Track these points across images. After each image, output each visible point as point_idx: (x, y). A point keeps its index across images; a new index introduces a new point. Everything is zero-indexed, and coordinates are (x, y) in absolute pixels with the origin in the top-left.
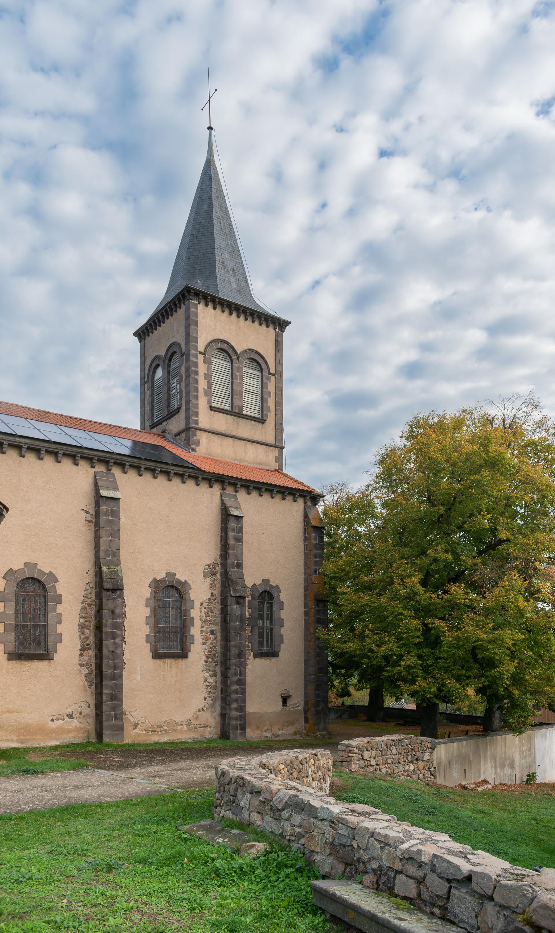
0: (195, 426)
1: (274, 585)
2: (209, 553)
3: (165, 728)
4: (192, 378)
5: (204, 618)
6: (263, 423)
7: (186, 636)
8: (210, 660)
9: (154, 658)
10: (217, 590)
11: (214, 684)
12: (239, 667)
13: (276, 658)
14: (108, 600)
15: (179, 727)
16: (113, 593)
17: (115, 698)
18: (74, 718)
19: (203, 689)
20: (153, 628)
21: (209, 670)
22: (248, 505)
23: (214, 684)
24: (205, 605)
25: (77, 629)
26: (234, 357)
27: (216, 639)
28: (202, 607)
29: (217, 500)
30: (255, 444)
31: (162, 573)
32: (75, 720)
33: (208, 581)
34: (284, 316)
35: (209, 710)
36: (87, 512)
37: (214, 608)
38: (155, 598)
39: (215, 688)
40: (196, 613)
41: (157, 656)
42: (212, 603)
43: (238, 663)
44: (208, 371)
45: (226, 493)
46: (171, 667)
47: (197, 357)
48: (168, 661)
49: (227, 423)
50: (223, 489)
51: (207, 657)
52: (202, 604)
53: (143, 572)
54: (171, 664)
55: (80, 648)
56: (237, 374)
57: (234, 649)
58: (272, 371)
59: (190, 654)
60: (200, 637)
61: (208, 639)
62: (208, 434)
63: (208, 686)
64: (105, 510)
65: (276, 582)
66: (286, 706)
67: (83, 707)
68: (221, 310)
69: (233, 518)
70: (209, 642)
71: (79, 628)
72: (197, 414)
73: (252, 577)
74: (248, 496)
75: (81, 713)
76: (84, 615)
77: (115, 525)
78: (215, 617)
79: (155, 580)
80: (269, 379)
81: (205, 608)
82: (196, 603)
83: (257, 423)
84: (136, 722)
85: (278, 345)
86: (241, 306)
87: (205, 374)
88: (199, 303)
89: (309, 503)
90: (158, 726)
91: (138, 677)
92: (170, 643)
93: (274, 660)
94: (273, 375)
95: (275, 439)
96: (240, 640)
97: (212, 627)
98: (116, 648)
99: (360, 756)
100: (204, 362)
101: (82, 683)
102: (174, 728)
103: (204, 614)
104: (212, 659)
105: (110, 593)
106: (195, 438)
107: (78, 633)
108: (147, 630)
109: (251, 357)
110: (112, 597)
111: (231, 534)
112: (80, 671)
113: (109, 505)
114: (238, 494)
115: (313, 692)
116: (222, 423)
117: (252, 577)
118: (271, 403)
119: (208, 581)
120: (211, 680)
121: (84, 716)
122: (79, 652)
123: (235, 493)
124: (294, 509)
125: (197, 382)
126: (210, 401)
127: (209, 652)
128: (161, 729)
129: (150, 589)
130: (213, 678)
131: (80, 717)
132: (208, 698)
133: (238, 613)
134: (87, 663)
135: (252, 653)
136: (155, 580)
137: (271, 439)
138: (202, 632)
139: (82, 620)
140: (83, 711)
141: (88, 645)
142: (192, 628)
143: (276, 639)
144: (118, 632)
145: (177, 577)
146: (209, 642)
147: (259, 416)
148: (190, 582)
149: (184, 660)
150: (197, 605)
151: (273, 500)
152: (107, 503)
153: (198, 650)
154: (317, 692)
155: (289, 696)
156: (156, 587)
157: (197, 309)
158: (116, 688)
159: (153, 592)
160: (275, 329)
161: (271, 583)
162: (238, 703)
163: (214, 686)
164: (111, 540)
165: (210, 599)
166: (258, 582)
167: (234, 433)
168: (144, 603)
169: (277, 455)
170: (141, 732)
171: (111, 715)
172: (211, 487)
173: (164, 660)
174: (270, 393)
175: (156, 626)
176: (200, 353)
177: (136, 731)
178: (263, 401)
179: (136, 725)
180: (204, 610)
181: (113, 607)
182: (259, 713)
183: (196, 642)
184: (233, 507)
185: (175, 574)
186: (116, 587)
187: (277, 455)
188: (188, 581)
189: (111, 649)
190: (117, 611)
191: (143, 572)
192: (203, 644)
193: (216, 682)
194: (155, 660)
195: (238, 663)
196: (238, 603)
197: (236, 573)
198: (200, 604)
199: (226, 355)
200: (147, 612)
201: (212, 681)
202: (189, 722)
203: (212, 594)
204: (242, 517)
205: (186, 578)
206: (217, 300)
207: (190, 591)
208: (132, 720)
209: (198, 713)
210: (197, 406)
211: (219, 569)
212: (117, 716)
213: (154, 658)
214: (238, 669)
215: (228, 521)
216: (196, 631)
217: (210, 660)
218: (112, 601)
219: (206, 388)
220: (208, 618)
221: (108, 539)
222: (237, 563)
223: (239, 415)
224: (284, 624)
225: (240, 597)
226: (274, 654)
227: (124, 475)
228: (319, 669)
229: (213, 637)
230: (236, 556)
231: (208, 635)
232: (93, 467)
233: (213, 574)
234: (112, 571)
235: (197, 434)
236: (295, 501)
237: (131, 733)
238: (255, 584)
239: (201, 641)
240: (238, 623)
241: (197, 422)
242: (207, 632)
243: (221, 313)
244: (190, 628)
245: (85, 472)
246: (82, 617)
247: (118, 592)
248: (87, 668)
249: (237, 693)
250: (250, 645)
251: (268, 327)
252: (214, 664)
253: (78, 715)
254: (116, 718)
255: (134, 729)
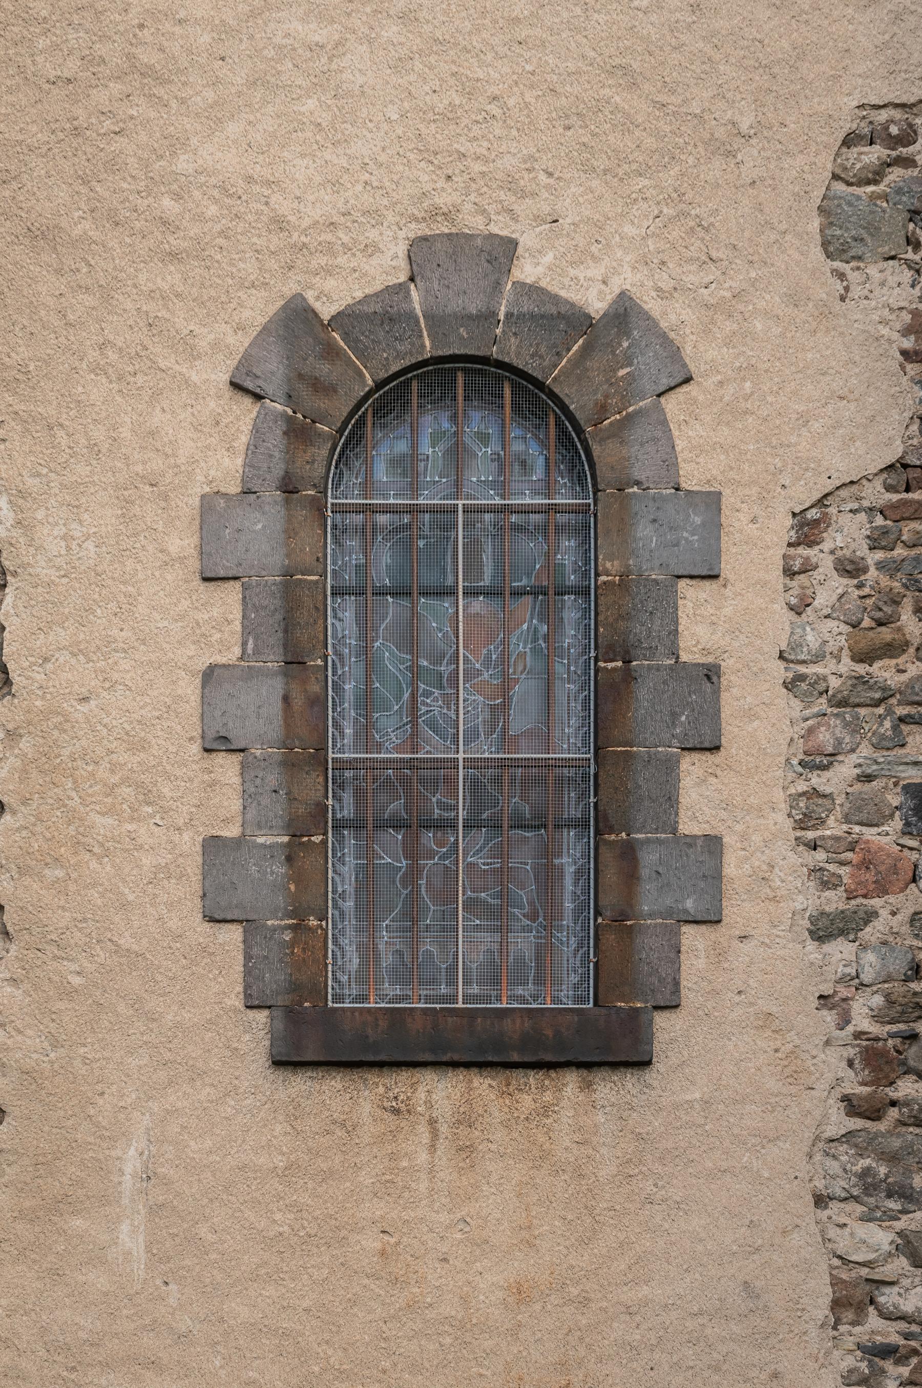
5: (837, 671)
7: (629, 852)
20: (273, 778)
24: (848, 533)
28: (822, 557)
41: (318, 1039)
45: (605, 840)
46: (466, 1150)
48: (439, 1092)
52: (808, 529)
53: (174, 256)
59: (665, 1026)
60: (790, 863)
63: (887, 1352)
70: (891, 914)
79: (297, 318)
81: (851, 568)
82: (737, 520)
91: (130, 1238)
99: (368, 1147)
103: (834, 633)
108: (220, 798)
129: (245, 412)
136: (297, 318)
138: (808, 814)
142: (692, 768)
145: (527, 270)
146: (891, 914)
147: (566, 992)
148: (673, 315)
149: (610, 1089)
150: (754, 540)
156: (305, 384)
159: (275, 440)
168: (183, 543)
173: (399, 1083)
180: (830, 589)
183: (738, 910)
185: (503, 251)
188: (652, 305)
191: (174, 256)
192: (825, 929)
194: (300, 1084)
198: (782, 528)
200: (219, 625)
205: (627, 279)
220: (884, 671)
239: (810, 900)
242: (868, 814)
244: (670, 767)
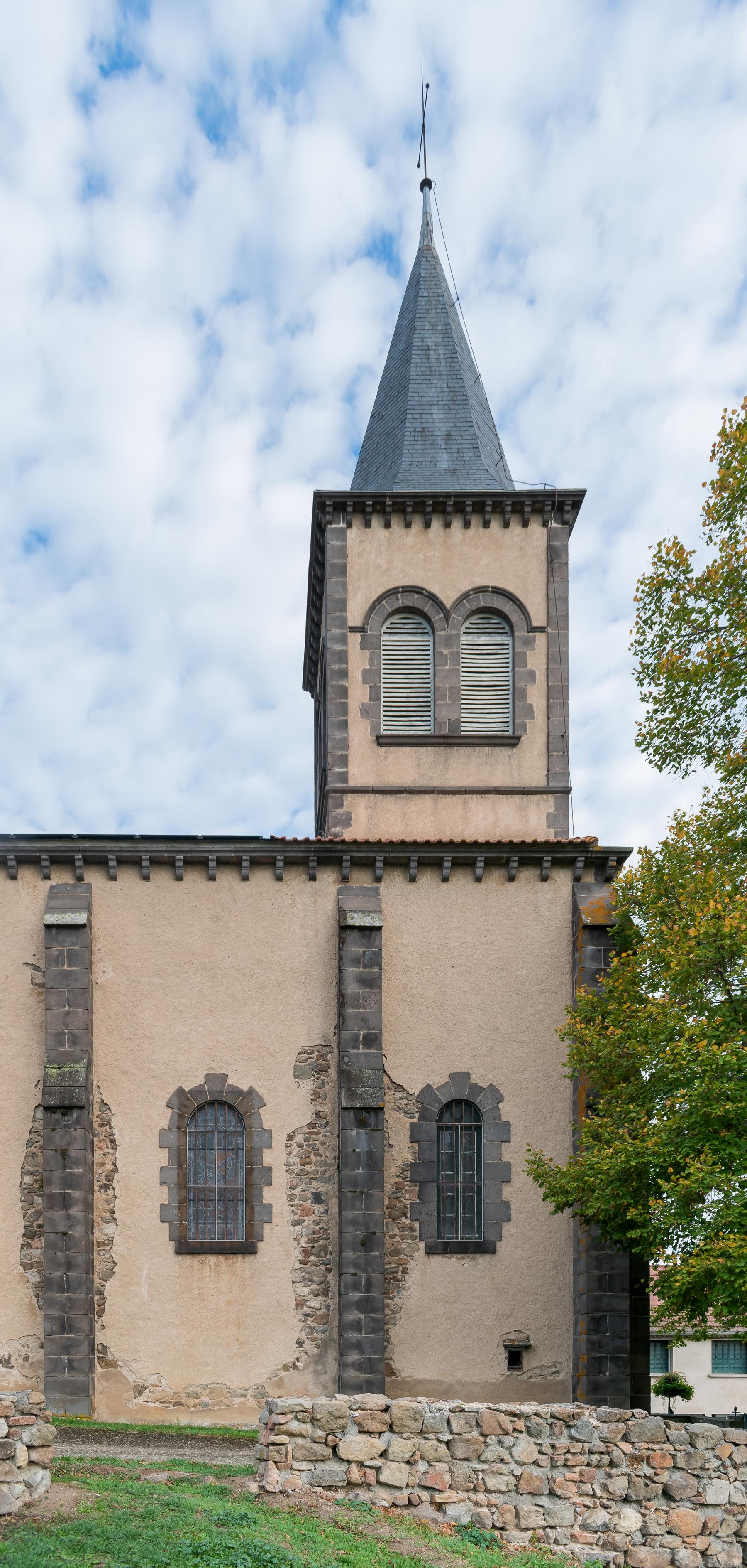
0: (339, 785)
1: (484, 1085)
2: (304, 1021)
3: (206, 1400)
4: (333, 687)
5: (297, 1168)
6: (514, 745)
8: (313, 1258)
9: (178, 1252)
10: (329, 1105)
11: (323, 1311)
12: (365, 1271)
13: (488, 1257)
14: (53, 1130)
15: (237, 1400)
16: (64, 1115)
17: (70, 1326)
18: (12, 1367)
19: (295, 1322)
20: (175, 1191)
21: (311, 1281)
22: (414, 915)
23: (323, 1311)
24: (299, 1138)
25: (16, 1194)
26: (437, 618)
27: (326, 1212)
29: (328, 906)
30: (492, 797)
31: (197, 1076)
32: (15, 1371)
33: (308, 1086)
34: (566, 483)
35: (311, 1368)
36: (36, 968)
37: (322, 1144)
38: (179, 1128)
39: (324, 1320)
40: (275, 1157)
41: (185, 1248)
42: (318, 1133)
43: (361, 1262)
44: (371, 664)
45: (352, 888)
46: (218, 1271)
47: (343, 640)
48: (212, 1259)
49: (419, 766)
50: (345, 879)
51: (306, 1252)
52: (291, 1137)
54: (217, 1265)
55: (23, 1231)
56: (445, 652)
57: (350, 1229)
58: (538, 618)
59: (261, 1246)
60: (287, 1210)
61: (306, 1212)
62: (372, 797)
63: (308, 1315)
64: (56, 953)
65: (490, 1076)
66: (519, 1369)
67: (30, 1346)
68: (402, 523)
69: (355, 934)
70: (309, 1221)
71: (24, 1195)
72: (344, 760)
73: (416, 1061)
74: (412, 887)
75: (26, 1359)
76: (32, 1169)
77: (76, 980)
78: (326, 1164)
79: (180, 1092)
80: (529, 643)
81: (300, 1146)
82: (275, 1135)
83: (497, 750)
84: (140, 1382)
85: (556, 559)
86: (448, 495)
87: (365, 673)
88: (349, 525)
89: (589, 878)
90: (188, 1395)
91: (144, 1291)
92: (214, 1220)
93: (483, 1260)
94: (541, 630)
95: (547, 776)
96: (367, 1209)
97: (317, 1186)
98: (71, 1227)
100: (363, 647)
101: (27, 1301)
102: (226, 1401)
103: (297, 1160)
104: (318, 1256)
105: (58, 1116)
106: (340, 811)
107: (20, 1204)
108: (163, 1195)
109: (482, 604)
110: (63, 1124)
111: (351, 971)
112: (22, 1276)
113: (65, 941)
114: (382, 886)
115: (585, 1337)
116: (406, 766)
117: (416, 1061)
118: (536, 696)
119: (308, 1086)
120: (315, 1303)
121: (32, 1364)
122: (21, 1241)
123: (375, 885)
124: (544, 905)
125: (344, 692)
126: (375, 727)
127: (312, 1241)
128: (196, 1401)
129: (169, 1112)
130: (320, 1298)
131: (23, 1366)
132: (307, 1341)
133: (362, 1146)
134: (38, 1262)
135: (422, 1245)
136: (180, 1092)
137: (536, 777)
139: (27, 1179)
140: (30, 1355)
141: (40, 1226)
142: (266, 1189)
143: (490, 1211)
144: (76, 1194)
145: (230, 1081)
146: (309, 1221)
148: (261, 1091)
149: (249, 1259)
150: (279, 1140)
151: (482, 886)
152: (60, 938)
153: (282, 1239)
154: (595, 1337)
155: (528, 1348)
156: (182, 1106)
157: (344, 539)
158: (71, 1308)
159: (176, 1118)
160: (545, 524)
161: (475, 1079)
162: (361, 1351)
163: (322, 1317)
164: (68, 1013)
165: (311, 1125)
166: (438, 1079)
167: (437, 783)
168: (156, 1140)
169: (552, 810)
170: (151, 1405)
171: (62, 1361)
172: (313, 878)
173: (203, 1257)
174: (532, 675)
175: (182, 1185)
176: (353, 630)
177: (139, 1400)
178: (517, 694)
179: (140, 1390)
180: (295, 1150)
181: (64, 1143)
182: (441, 1383)
184: (356, 911)
186: (67, 1103)
187: (552, 810)
188: (257, 1089)
189: (61, 1229)
190: (72, 1151)
193: (327, 1307)
194: (181, 1258)
195: (361, 1262)
196: (361, 1124)
197: (363, 1058)
198: (285, 1137)
199: (419, 620)
200: (163, 1158)
201: (317, 1305)
202: (262, 1390)
203: (318, 1115)
204: (379, 928)
206: (389, 502)
207: (261, 1111)
208: (131, 1379)
209: (283, 1373)
210: (344, 744)
211: (332, 1058)
212: (75, 1364)
213: (178, 1252)
214: (363, 1275)
215: (356, 944)
216: (275, 1196)
217: (313, 1258)
218: (62, 1132)
219: (367, 700)
220: (307, 1168)
221: (62, 1010)
222: (365, 1037)
223: (449, 740)
224: (513, 1177)
225: (368, 1110)
226: (484, 1247)
227: (112, 883)
228: (601, 1278)
229: (319, 1208)
230: (364, 1020)
231: (308, 1204)
232: (47, 877)
233: (321, 1070)
234: (65, 1073)
235: (345, 803)
236: (544, 879)
237: (130, 1405)
238: (428, 1086)
240: (361, 1170)
241: (344, 777)
243: (403, 531)
244: (261, 1189)
245: (31, 890)
246: (30, 1173)
247: (75, 1114)
248: (39, 1272)
249: (359, 1330)
250: (416, 1225)
251: (525, 524)
252: (323, 1267)
253: (20, 1361)
254: (71, 1368)
255: (135, 1398)
